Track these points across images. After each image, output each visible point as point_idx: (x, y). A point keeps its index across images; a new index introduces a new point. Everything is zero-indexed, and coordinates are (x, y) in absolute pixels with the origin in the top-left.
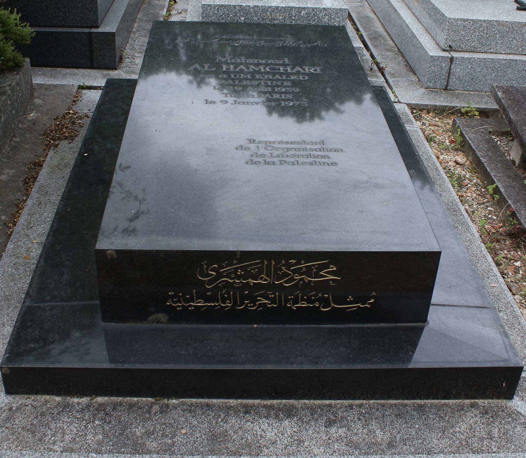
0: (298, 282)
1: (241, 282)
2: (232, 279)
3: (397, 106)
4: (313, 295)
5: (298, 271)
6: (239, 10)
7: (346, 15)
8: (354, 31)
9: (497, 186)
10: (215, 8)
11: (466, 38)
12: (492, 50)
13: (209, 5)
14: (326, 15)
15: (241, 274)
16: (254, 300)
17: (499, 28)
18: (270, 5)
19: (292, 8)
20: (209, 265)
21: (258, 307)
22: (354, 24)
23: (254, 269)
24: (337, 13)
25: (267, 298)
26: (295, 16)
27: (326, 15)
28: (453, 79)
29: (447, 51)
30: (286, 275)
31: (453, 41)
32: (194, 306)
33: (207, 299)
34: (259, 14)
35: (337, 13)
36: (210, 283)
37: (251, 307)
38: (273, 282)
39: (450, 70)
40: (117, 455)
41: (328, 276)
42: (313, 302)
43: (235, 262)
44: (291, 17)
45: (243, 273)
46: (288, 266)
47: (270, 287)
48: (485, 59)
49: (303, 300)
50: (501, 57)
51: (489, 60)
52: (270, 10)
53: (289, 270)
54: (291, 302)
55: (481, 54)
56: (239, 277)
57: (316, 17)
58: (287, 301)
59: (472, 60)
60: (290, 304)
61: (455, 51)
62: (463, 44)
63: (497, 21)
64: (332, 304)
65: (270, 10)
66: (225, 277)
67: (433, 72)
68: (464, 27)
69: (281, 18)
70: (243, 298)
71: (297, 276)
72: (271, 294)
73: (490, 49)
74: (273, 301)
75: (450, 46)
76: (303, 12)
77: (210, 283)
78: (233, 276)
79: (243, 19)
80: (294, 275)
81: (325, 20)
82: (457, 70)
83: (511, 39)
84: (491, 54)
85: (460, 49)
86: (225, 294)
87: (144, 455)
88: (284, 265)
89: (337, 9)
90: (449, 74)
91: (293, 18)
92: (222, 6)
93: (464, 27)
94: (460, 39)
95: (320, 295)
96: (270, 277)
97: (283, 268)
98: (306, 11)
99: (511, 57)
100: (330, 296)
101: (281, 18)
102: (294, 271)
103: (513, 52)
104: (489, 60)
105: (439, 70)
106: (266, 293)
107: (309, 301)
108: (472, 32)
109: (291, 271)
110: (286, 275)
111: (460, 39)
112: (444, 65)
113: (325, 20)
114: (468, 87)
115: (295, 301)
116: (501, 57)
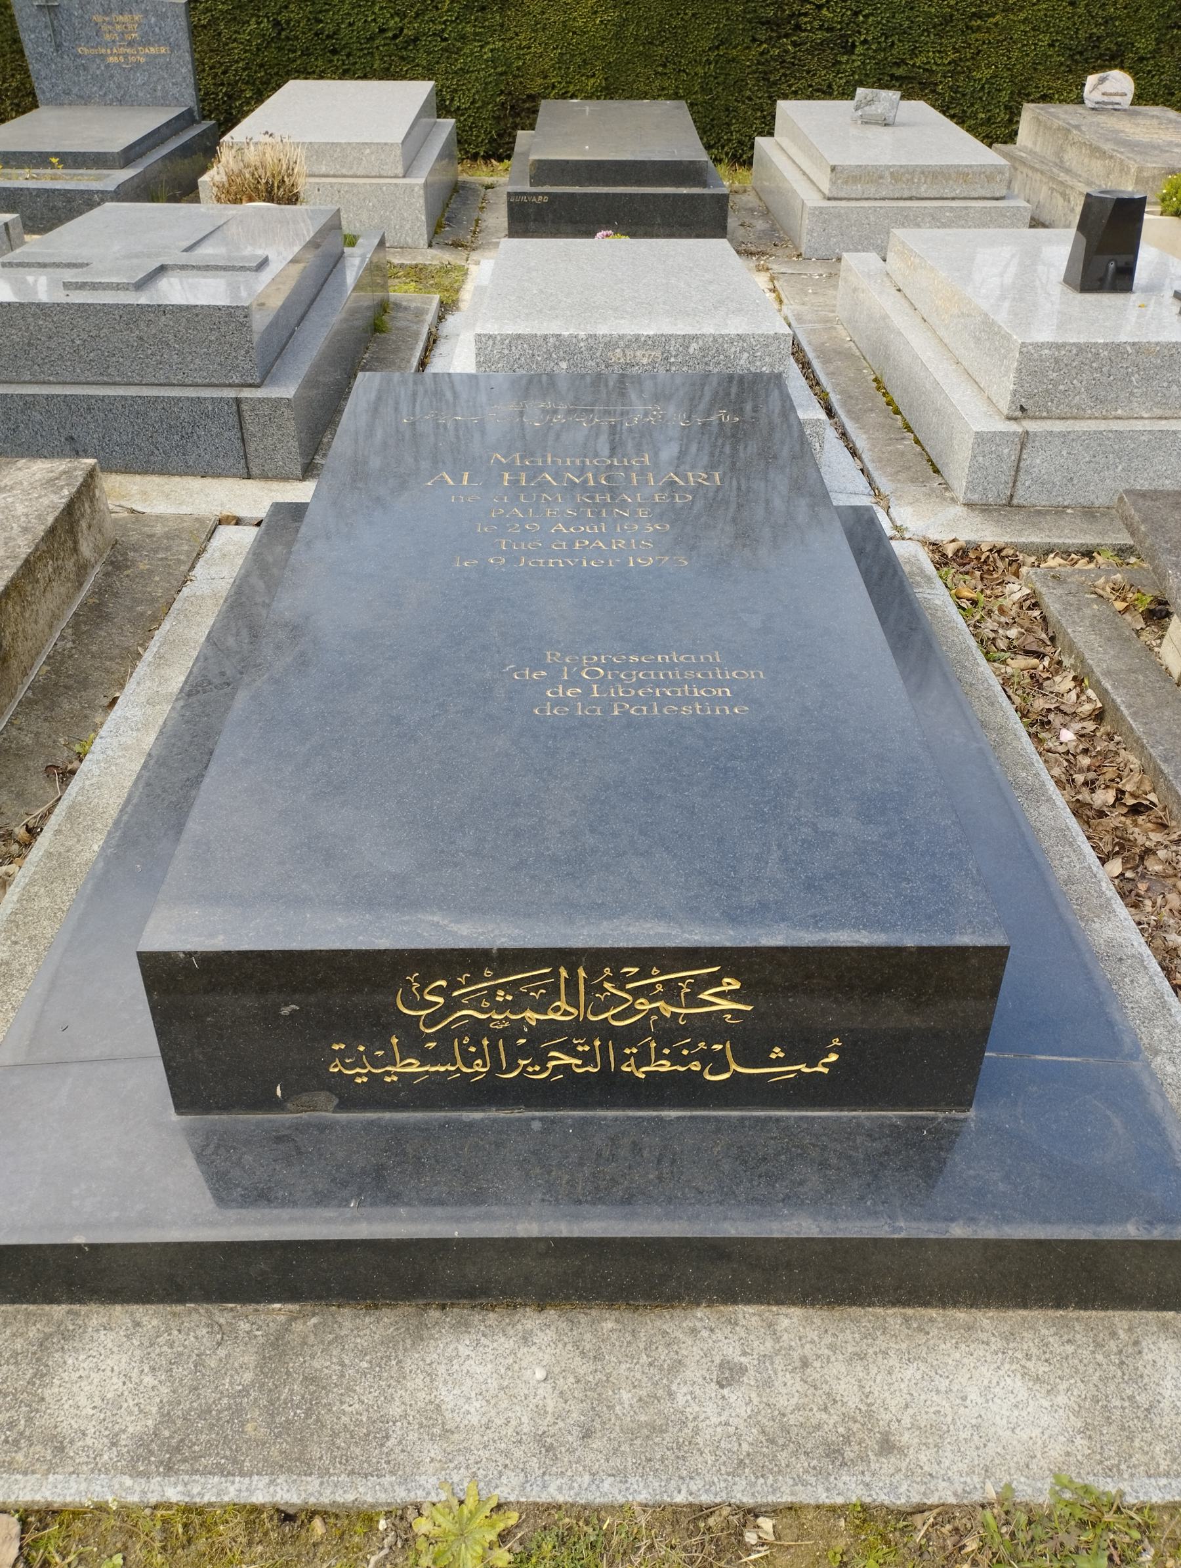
1: (506, 1018)
2: (482, 1011)
3: (901, 549)
4: (684, 1046)
5: (645, 992)
6: (555, 346)
7: (788, 348)
8: (803, 382)
10: (502, 343)
11: (1061, 387)
12: (1119, 412)
13: (490, 336)
14: (743, 350)
15: (505, 1000)
16: (541, 1059)
18: (621, 333)
19: (668, 338)
20: (424, 982)
21: (552, 1075)
22: (805, 365)
23: (536, 989)
24: (767, 346)
25: (571, 1051)
26: (675, 356)
27: (743, 350)
28: (1025, 480)
29: (1015, 419)
30: (615, 1000)
32: (396, 1073)
33: (426, 1057)
34: (598, 354)
35: (767, 346)
36: (431, 1020)
37: (535, 1073)
38: (585, 1017)
39: (1019, 462)
40: (186, 1478)
41: (720, 1001)
42: (685, 1061)
43: (487, 973)
44: (667, 359)
45: (509, 998)
46: (620, 980)
47: (582, 1028)
48: (1101, 433)
49: (660, 1056)
50: (1139, 425)
51: (1110, 435)
52: (621, 344)
53: (622, 989)
54: (632, 1060)
55: (1093, 422)
56: (501, 1007)
57: (722, 357)
58: (622, 1059)
59: (1072, 436)
60: (629, 1066)
61: (1034, 418)
62: (1052, 401)
63: (1134, 344)
64: (734, 1066)
65: (621, 344)
66: (465, 1007)
67: (980, 468)
68: (1057, 361)
69: (645, 361)
70: (515, 1054)
71: (642, 1004)
72: (582, 1045)
73: (1116, 409)
74: (588, 1058)
75: (1022, 409)
76: (693, 347)
77: (431, 1020)
78: (485, 1004)
79: (564, 365)
80: (634, 1001)
81: (742, 362)
82: (1036, 461)
83: (1165, 384)
84: (1116, 421)
85: (1045, 414)
86: (468, 1045)
87: (256, 1478)
88: (608, 979)
89: (768, 337)
90: (1017, 471)
91: (672, 360)
92: (519, 336)
93: (1057, 361)
94: (1047, 390)
95: (702, 1045)
97: (607, 985)
98: (701, 342)
99: (1163, 425)
100: (728, 1045)
101: (645, 361)
102: (637, 993)
104: (1110, 435)
105: (995, 462)
106: (569, 1041)
107: (676, 1058)
108: (1073, 372)
109: (628, 991)
110: (615, 1000)
111: (1047, 390)
112: (1006, 451)
113: (742, 362)
114: (1060, 499)
115: (643, 1059)
116: (1139, 425)
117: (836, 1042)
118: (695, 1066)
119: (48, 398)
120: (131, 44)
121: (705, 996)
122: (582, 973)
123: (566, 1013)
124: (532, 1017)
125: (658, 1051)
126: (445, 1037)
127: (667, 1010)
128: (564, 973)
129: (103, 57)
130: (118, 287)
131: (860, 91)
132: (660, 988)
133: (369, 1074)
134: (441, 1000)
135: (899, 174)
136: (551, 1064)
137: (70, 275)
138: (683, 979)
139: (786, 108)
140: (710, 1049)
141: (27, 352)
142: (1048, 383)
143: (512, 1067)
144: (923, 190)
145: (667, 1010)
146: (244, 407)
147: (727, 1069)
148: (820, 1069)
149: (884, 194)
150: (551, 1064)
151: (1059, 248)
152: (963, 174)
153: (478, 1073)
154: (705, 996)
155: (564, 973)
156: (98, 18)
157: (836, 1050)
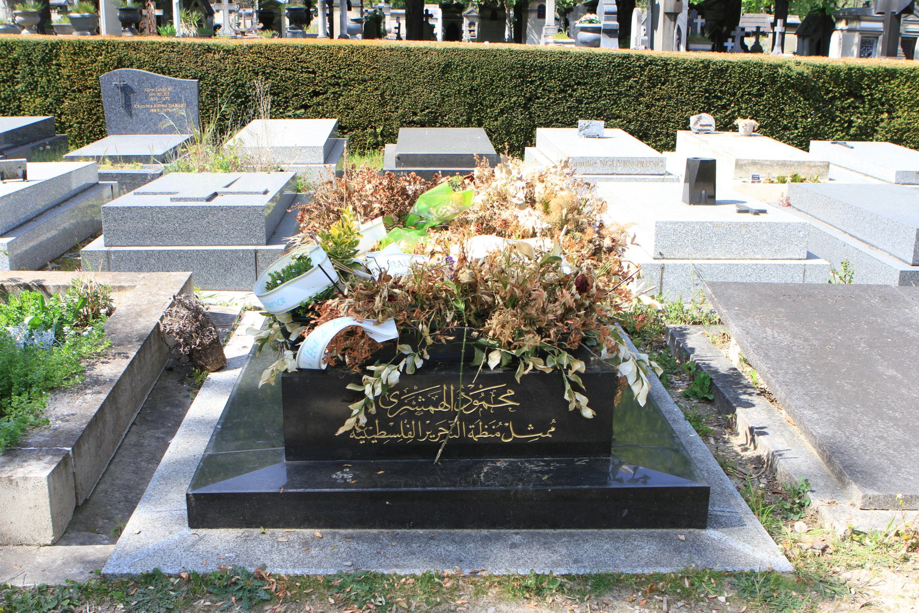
0: (478, 410)
2: (413, 406)
9: (433, 37)
17: (715, 229)
23: (434, 395)
30: (465, 401)
31: (664, 248)
37: (433, 438)
42: (493, 432)
56: (420, 405)
58: (468, 431)
64: (513, 434)
68: (674, 230)
78: (414, 403)
82: (669, 278)
90: (661, 284)
93: (674, 230)
96: (450, 404)
103: (734, 257)
110: (465, 401)
117: (554, 421)
118: (498, 435)
119: (160, 252)
120: (164, 103)
121: (500, 398)
122: (452, 388)
123: (446, 407)
124: (432, 409)
125: (483, 426)
126: (397, 420)
127: (486, 405)
128: (445, 388)
129: (149, 109)
130: (198, 200)
131: (581, 122)
132: (483, 395)
133: (366, 439)
134: (396, 401)
135: (605, 161)
136: (439, 434)
137: (172, 196)
138: (492, 390)
139: (542, 133)
140: (504, 426)
141: (150, 231)
142: (668, 234)
143: (424, 435)
144: (619, 170)
145: (486, 405)
146: (258, 254)
147: (510, 436)
148: (548, 435)
149: (598, 172)
150: (439, 434)
151: (679, 188)
152: (641, 162)
153: (410, 439)
154: (500, 398)
155: (445, 388)
156: (148, 90)
157: (554, 425)
